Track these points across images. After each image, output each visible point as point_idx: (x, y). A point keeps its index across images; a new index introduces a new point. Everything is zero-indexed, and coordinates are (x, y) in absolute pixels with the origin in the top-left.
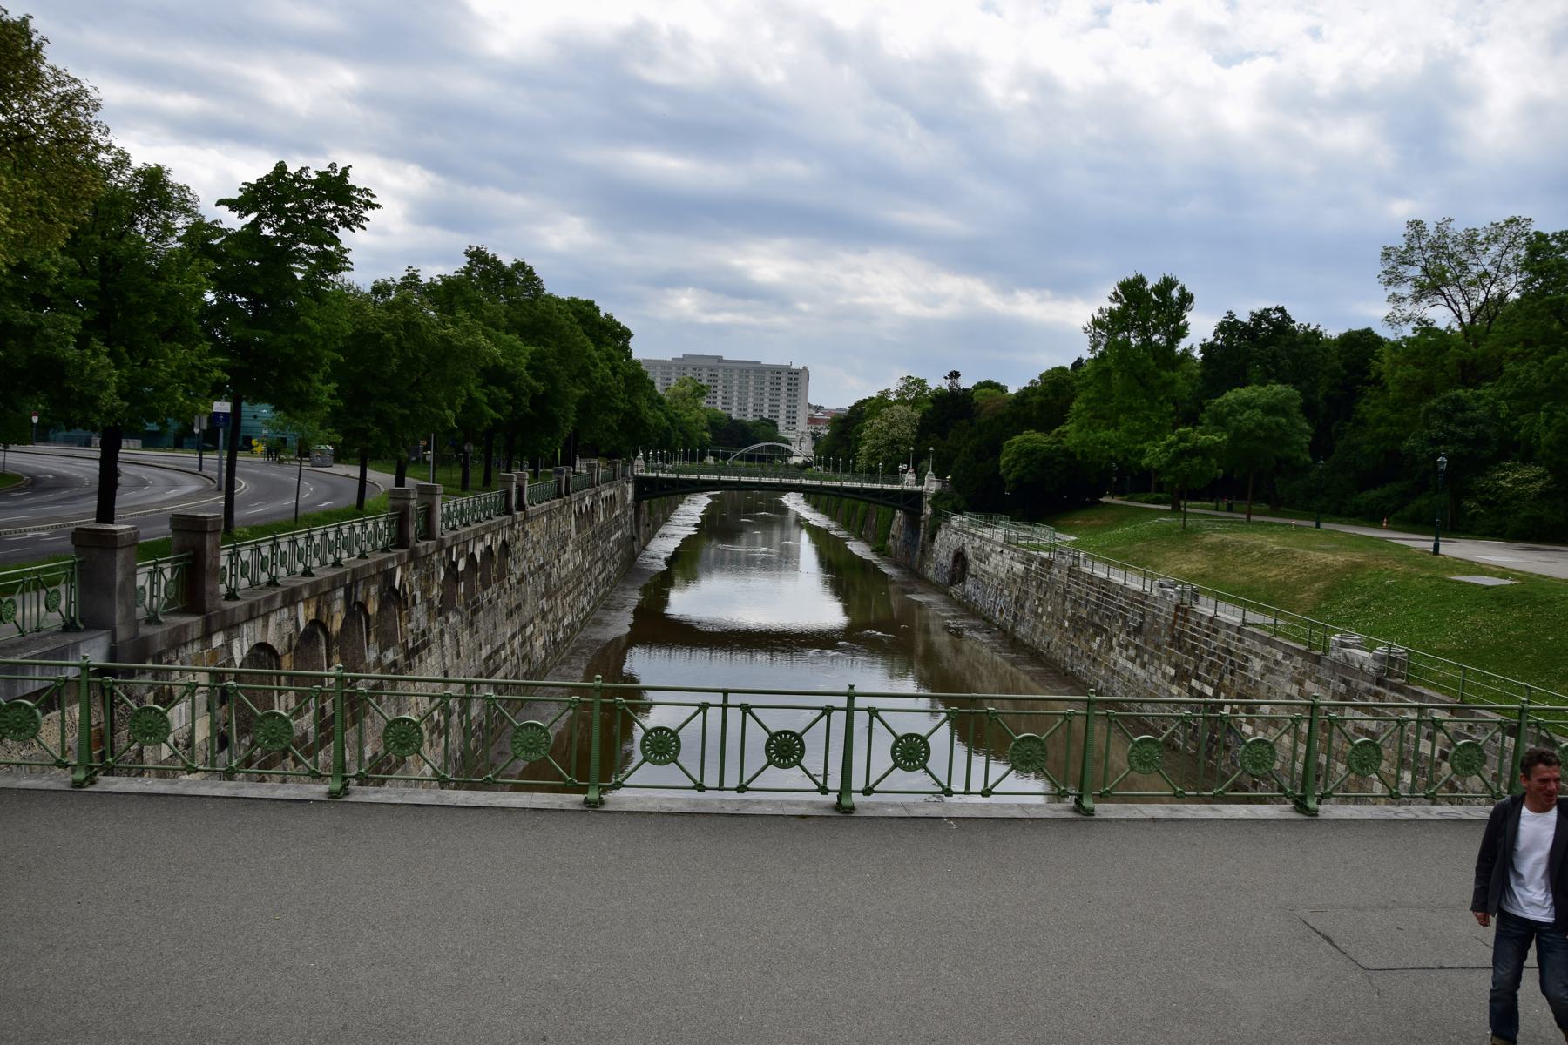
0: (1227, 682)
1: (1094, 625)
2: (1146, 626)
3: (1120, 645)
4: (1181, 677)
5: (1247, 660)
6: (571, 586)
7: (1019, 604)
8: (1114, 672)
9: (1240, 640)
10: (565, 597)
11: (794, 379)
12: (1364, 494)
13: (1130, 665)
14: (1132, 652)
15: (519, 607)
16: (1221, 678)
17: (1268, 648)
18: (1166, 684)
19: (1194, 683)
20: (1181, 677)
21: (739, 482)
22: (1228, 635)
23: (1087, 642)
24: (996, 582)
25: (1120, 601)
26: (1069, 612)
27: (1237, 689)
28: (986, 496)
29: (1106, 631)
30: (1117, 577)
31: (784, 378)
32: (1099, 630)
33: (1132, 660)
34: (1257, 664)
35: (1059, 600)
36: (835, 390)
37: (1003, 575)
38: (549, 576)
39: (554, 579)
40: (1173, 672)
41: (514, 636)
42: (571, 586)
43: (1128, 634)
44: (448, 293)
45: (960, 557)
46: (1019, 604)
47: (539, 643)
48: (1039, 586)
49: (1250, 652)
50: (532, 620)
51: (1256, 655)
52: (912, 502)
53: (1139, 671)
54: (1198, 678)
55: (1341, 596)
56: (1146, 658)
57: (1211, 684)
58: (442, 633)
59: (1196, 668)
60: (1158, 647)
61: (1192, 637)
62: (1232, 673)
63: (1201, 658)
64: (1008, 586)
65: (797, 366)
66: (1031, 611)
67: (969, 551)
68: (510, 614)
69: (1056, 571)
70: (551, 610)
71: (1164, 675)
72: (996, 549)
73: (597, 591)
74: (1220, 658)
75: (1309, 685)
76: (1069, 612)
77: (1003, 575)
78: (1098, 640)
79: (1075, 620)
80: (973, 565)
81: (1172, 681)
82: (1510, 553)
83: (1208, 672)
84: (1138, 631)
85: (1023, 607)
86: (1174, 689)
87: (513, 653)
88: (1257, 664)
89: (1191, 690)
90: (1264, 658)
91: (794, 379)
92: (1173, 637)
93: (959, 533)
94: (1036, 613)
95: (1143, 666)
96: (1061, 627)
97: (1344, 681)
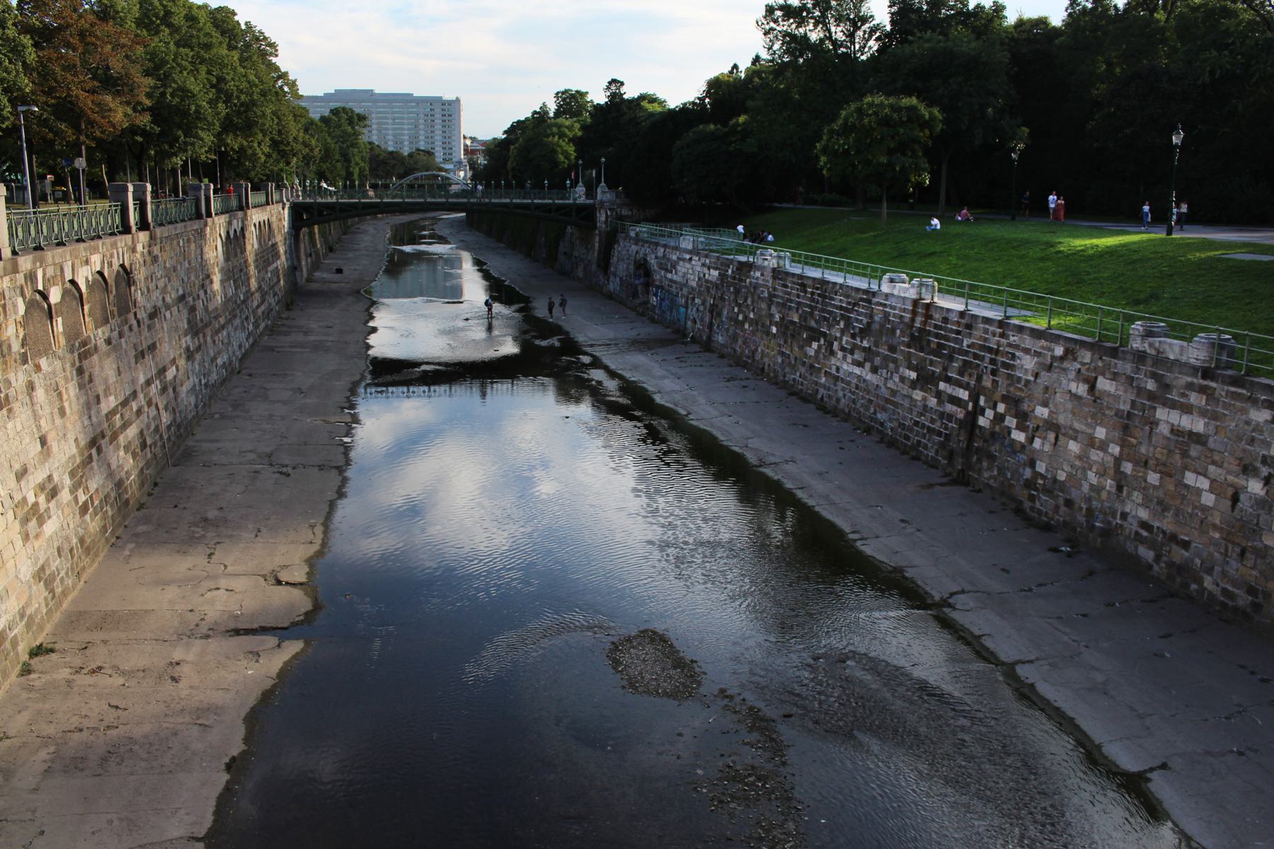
0: (987, 382)
1: (811, 329)
2: (875, 327)
3: (843, 349)
4: (926, 380)
5: (1013, 357)
6: (222, 320)
7: (714, 311)
8: (837, 379)
9: (1002, 335)
10: (217, 332)
11: (446, 111)
12: (249, 248)
13: (857, 371)
14: (858, 356)
15: (152, 347)
16: (979, 379)
17: (1043, 343)
18: (905, 389)
19: (942, 385)
20: (926, 380)
21: (426, 203)
22: (986, 331)
23: (801, 348)
24: (685, 291)
25: (839, 300)
26: (777, 317)
27: (1002, 390)
28: (673, 208)
29: (824, 335)
30: (835, 278)
31: (438, 110)
32: (815, 335)
33: (859, 364)
34: (1028, 363)
35: (764, 306)
36: (486, 120)
37: (694, 284)
38: (193, 309)
39: (200, 313)
40: (913, 375)
41: (148, 383)
42: (222, 320)
43: (853, 336)
44: (199, 7)
45: (642, 268)
46: (714, 311)
47: (184, 390)
48: (737, 291)
49: (1017, 347)
50: (173, 361)
51: (1027, 351)
52: (585, 215)
53: (869, 377)
54: (948, 380)
55: (1135, 285)
56: (877, 361)
57: (966, 387)
58: (31, 387)
59: (945, 369)
60: (893, 349)
61: (937, 336)
62: (994, 373)
63: (951, 358)
64: (700, 293)
65: (449, 96)
66: (731, 319)
67: (652, 260)
68: (141, 355)
69: (758, 274)
70: (199, 348)
71: (902, 379)
72: (689, 259)
73: (256, 326)
74: (976, 356)
75: (1104, 384)
76: (777, 317)
77: (694, 284)
78: (815, 345)
79: (784, 325)
80: (658, 275)
81: (914, 384)
82: (1241, 231)
83: (961, 373)
84: (864, 332)
85: (719, 315)
86: (918, 395)
87: (149, 403)
88: (1028, 363)
89: (939, 395)
90: (1037, 354)
91: (446, 111)
92: (912, 336)
93: (640, 241)
94: (736, 321)
95: (874, 370)
96: (768, 333)
97: (1154, 376)
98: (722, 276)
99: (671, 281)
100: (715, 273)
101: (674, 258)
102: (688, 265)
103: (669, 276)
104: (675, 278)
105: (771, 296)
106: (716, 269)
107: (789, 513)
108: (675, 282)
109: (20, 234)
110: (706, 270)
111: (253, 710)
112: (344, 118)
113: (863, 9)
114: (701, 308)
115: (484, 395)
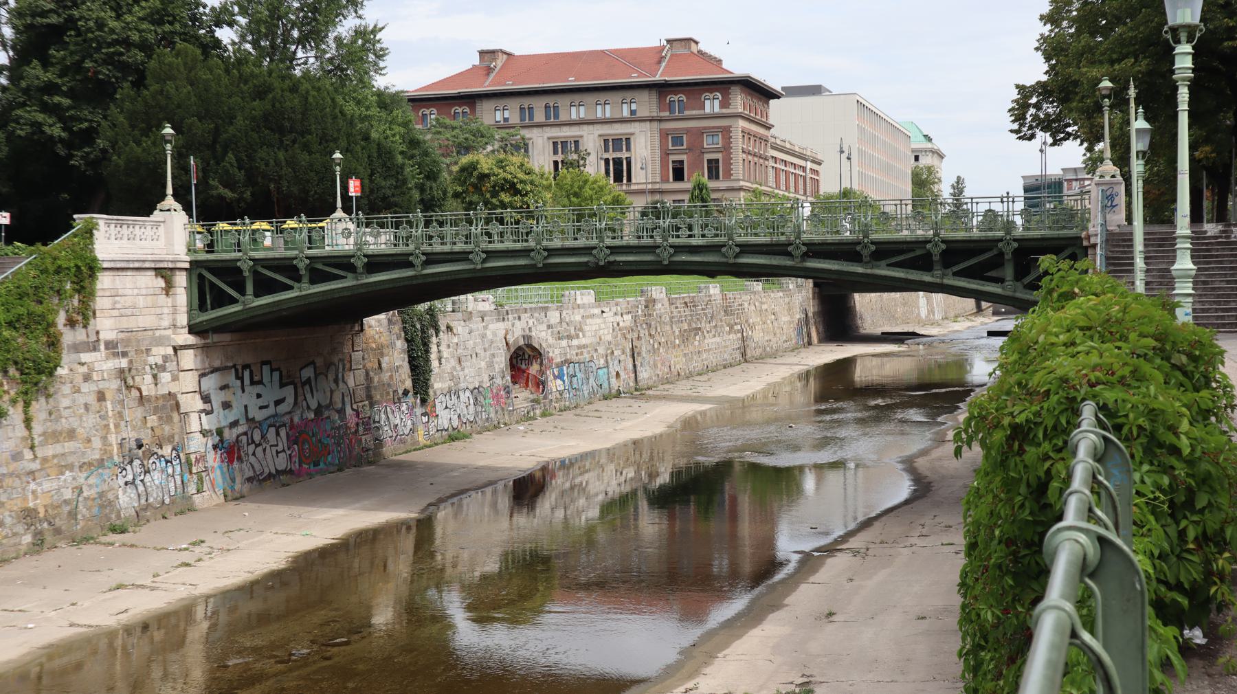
35: (668, 328)
37: (609, 338)
64: (617, 345)
98: (635, 318)
99: (579, 347)
100: (628, 317)
101: (578, 318)
102: (599, 321)
103: (575, 342)
104: (583, 341)
105: (671, 318)
106: (628, 313)
107: (383, 617)
108: (584, 347)
109: (172, 484)
110: (619, 318)
111: (668, 666)
112: (1051, 49)
113: (821, 193)
114: (622, 358)
115: (1037, 49)
